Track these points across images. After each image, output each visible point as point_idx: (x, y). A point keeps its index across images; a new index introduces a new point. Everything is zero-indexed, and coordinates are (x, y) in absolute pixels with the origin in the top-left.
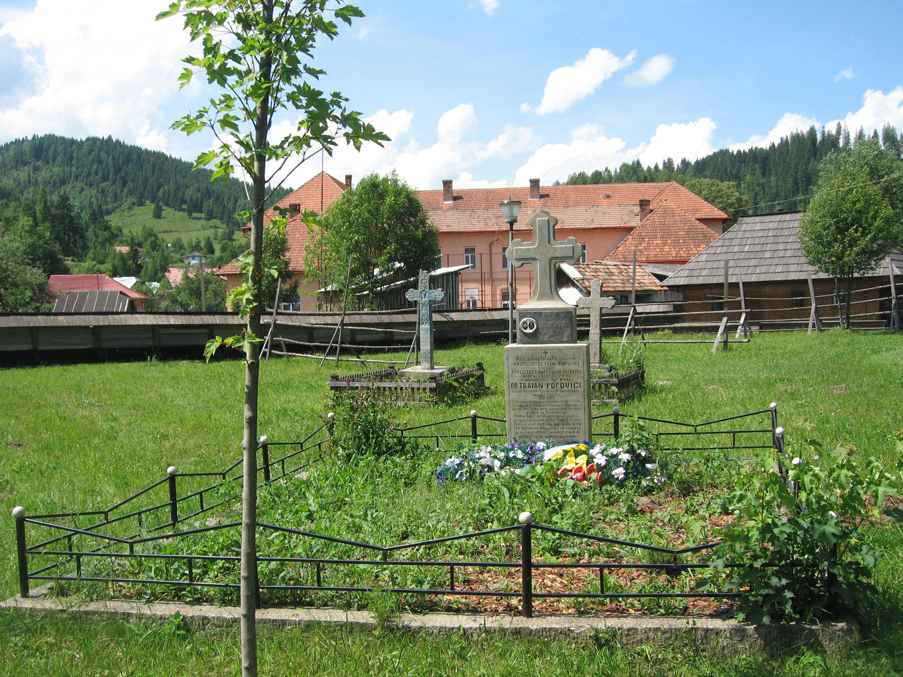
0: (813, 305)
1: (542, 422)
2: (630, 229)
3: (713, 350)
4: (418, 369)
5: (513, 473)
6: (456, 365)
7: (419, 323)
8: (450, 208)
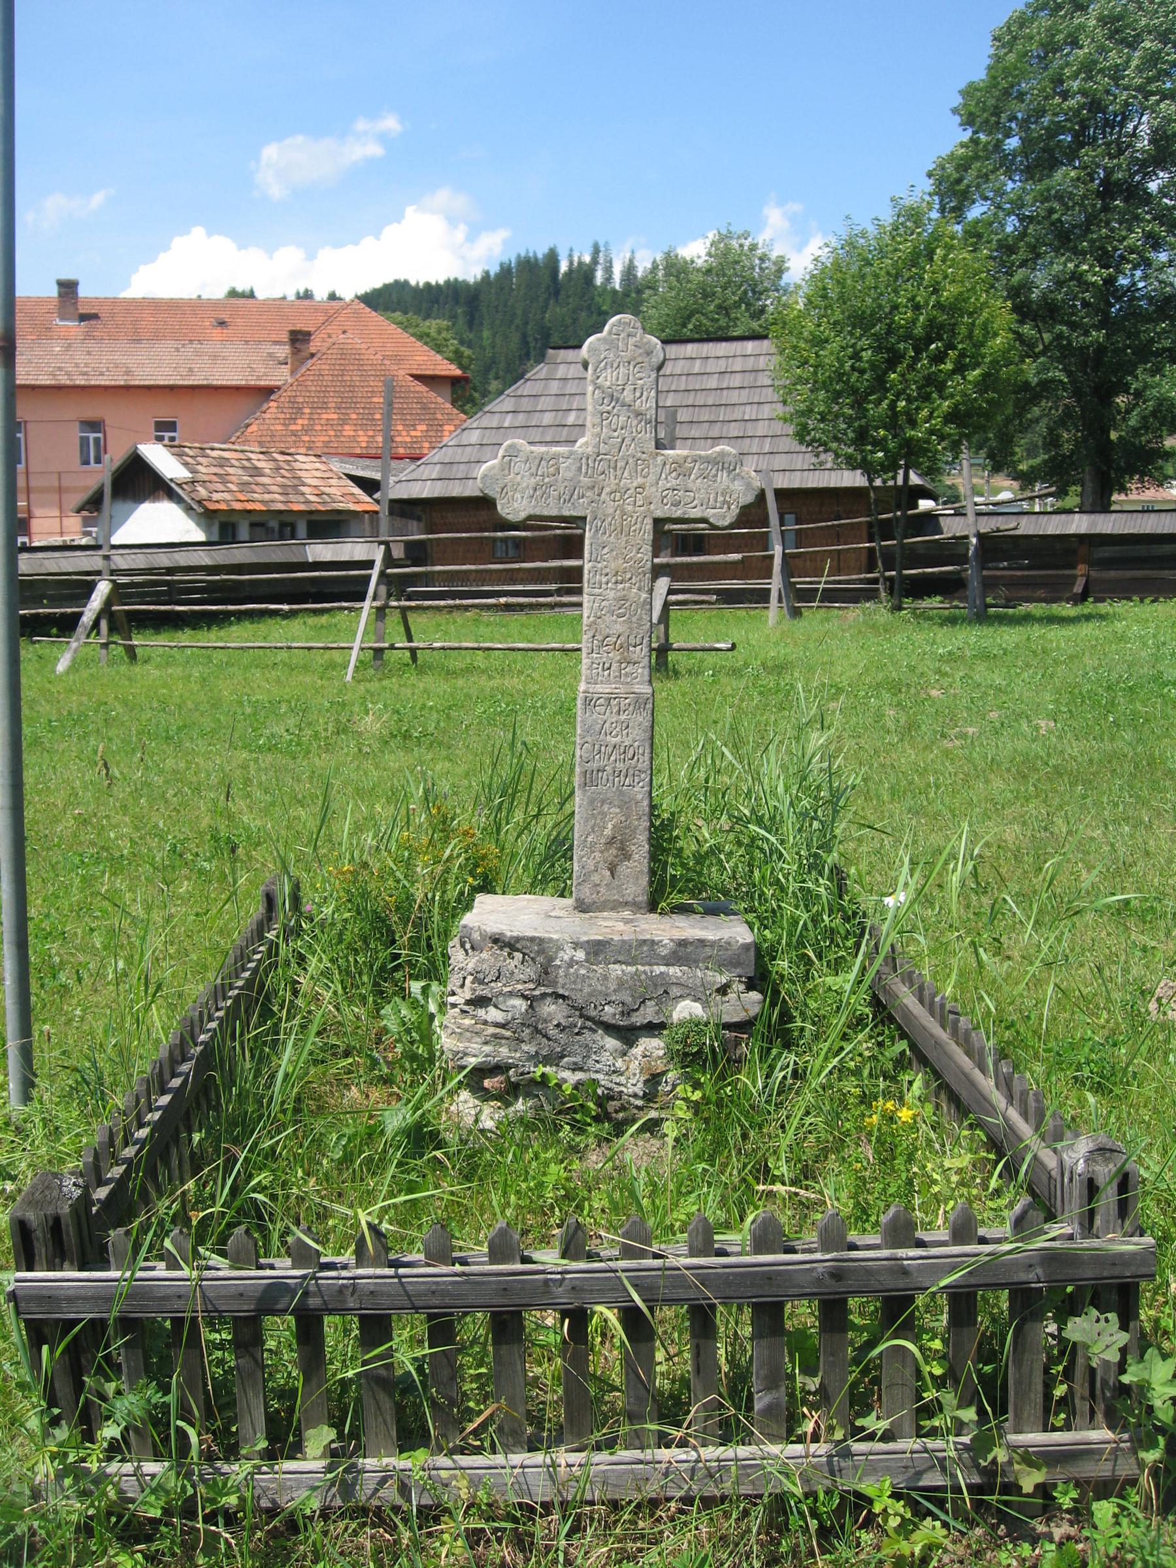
2: (267, 392)
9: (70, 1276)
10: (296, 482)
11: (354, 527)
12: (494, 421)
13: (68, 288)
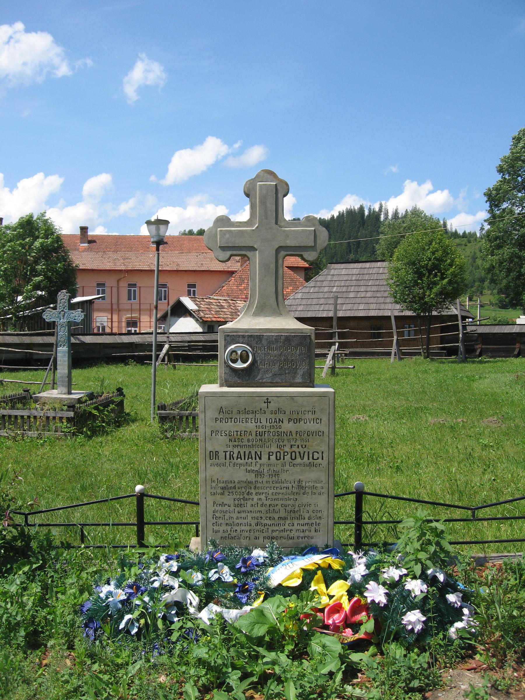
0: (395, 338)
1: (258, 515)
4: (55, 393)
5: (220, 616)
6: (95, 388)
7: (57, 345)
8: (85, 250)
9: (163, 412)
10: (236, 311)
13: (84, 230)
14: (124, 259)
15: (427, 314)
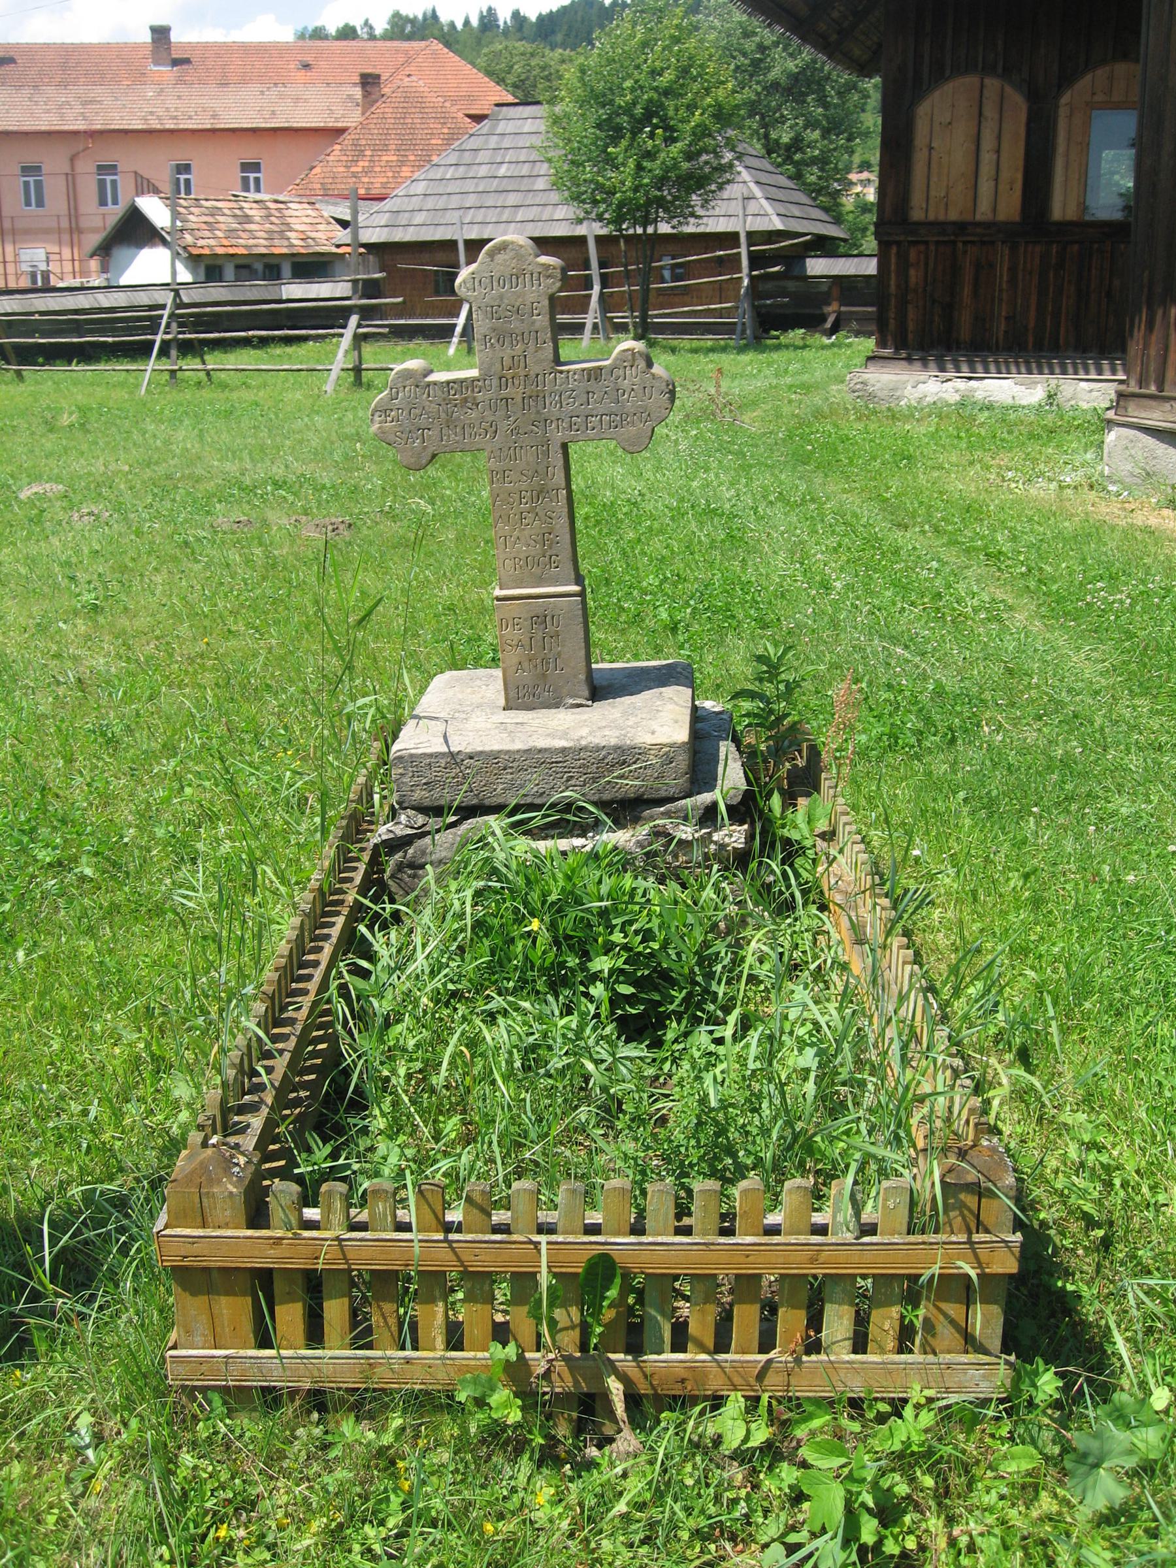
2: (341, 131)
3: (329, 387)
10: (283, 228)
11: (338, 267)
12: (437, 174)
13: (161, 34)
14: (85, 103)
15: (640, 231)
